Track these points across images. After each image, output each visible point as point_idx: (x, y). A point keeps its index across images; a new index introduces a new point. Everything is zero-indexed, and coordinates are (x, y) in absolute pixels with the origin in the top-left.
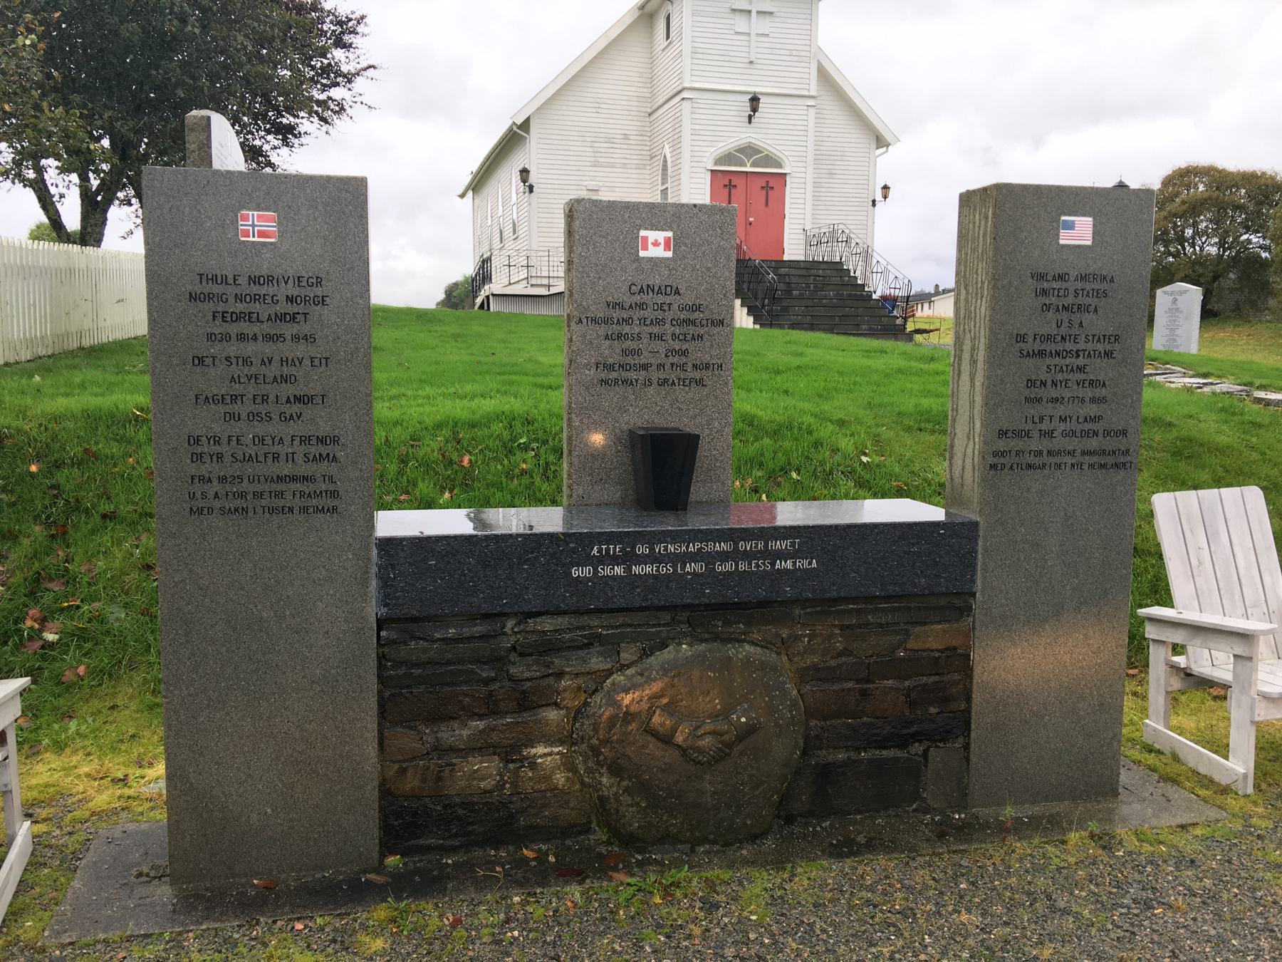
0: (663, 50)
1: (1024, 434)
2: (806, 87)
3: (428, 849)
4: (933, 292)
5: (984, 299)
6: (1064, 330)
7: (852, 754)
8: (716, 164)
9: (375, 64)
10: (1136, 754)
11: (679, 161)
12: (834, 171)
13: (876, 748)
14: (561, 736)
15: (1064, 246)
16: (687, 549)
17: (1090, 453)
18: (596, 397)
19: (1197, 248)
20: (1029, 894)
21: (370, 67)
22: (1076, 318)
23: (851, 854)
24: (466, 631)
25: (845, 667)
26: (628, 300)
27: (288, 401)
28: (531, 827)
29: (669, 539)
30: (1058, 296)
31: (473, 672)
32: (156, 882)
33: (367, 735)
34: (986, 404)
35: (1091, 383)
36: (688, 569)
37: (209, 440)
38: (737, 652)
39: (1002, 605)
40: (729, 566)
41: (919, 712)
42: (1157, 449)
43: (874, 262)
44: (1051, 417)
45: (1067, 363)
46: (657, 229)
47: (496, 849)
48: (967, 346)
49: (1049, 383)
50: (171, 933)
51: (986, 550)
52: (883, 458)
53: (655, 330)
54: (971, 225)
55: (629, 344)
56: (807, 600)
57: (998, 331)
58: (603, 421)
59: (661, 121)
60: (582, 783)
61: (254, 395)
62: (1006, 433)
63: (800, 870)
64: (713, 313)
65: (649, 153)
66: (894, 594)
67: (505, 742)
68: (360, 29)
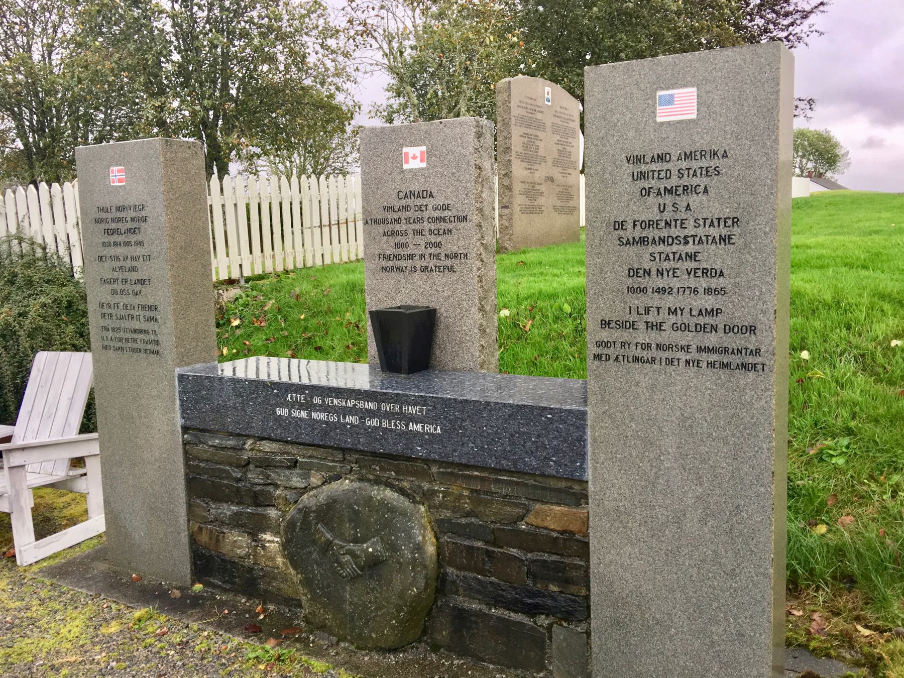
1: (624, 325)
6: (668, 215)
7: (484, 607)
15: (662, 124)
17: (708, 350)
22: (682, 201)
26: (397, 204)
30: (659, 178)
35: (705, 272)
36: (347, 420)
39: (615, 500)
40: (374, 422)
44: (658, 308)
45: (674, 250)
49: (654, 272)
51: (595, 440)
53: (417, 227)
55: (399, 239)
57: (594, 219)
62: (609, 324)
66: (507, 468)
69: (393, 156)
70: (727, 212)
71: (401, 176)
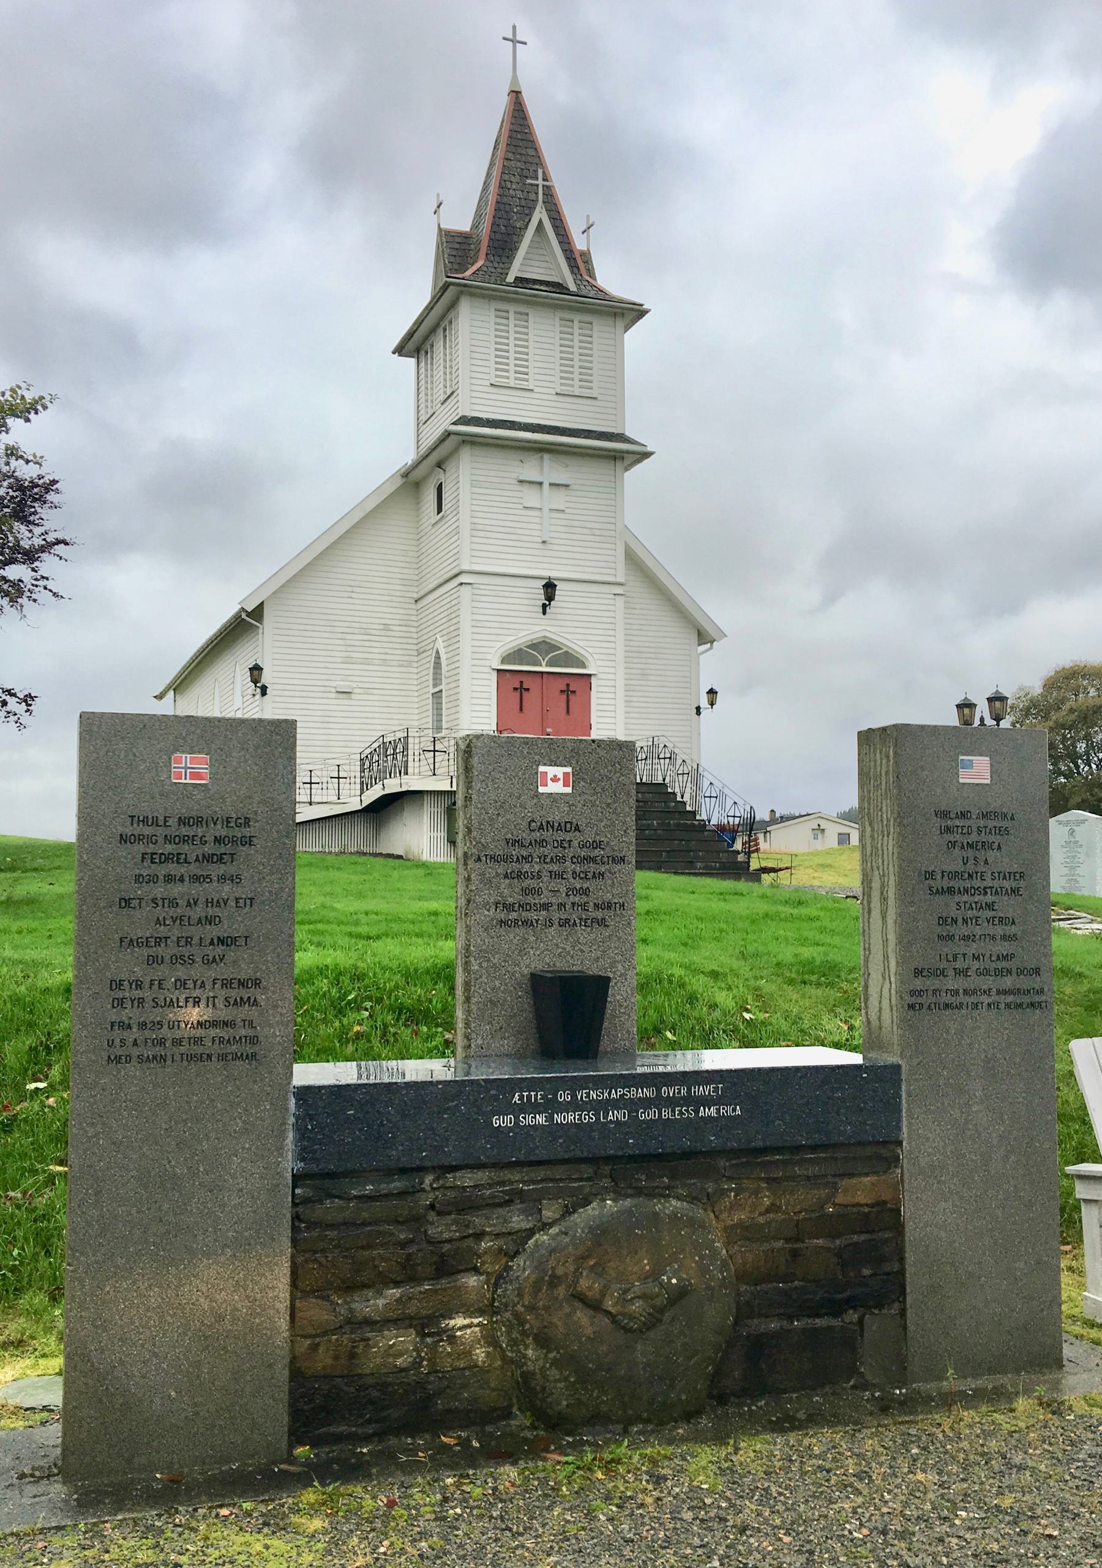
0: (433, 525)
2: (613, 571)
3: (338, 1438)
4: (767, 819)
5: (891, 837)
6: (970, 867)
8: (502, 662)
9: (68, 539)
10: (1077, 1329)
11: (456, 658)
12: (648, 672)
13: (809, 1316)
14: (481, 1305)
16: (610, 1096)
17: (1005, 992)
18: (495, 939)
19: (1094, 767)
20: (983, 1454)
21: (58, 542)
22: (981, 855)
23: (793, 1428)
24: (384, 1188)
25: (774, 1225)
26: (526, 836)
27: (212, 943)
28: (449, 1411)
29: (591, 1085)
30: (962, 833)
31: (392, 1234)
32: (45, 1481)
33: (278, 1305)
34: (899, 942)
35: (1001, 920)
37: (131, 985)
38: (664, 1208)
40: (652, 1114)
41: (852, 1274)
42: (1068, 1002)
43: (706, 784)
44: (964, 955)
46: (556, 765)
47: (413, 1438)
48: (876, 884)
49: (960, 920)
50: (86, 1524)
52: (767, 1015)
53: (555, 867)
54: (872, 763)
56: (732, 1150)
58: (503, 964)
59: (431, 610)
60: (504, 1358)
61: (178, 938)
62: (922, 972)
63: (743, 1444)
64: (614, 850)
65: (415, 647)
67: (424, 1312)
68: (51, 497)
69: (524, 774)
70: (1015, 867)
71: (535, 801)
